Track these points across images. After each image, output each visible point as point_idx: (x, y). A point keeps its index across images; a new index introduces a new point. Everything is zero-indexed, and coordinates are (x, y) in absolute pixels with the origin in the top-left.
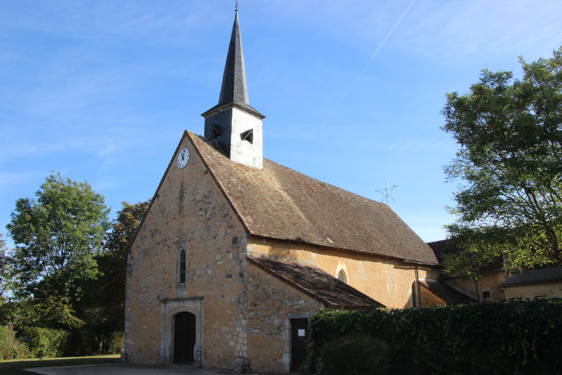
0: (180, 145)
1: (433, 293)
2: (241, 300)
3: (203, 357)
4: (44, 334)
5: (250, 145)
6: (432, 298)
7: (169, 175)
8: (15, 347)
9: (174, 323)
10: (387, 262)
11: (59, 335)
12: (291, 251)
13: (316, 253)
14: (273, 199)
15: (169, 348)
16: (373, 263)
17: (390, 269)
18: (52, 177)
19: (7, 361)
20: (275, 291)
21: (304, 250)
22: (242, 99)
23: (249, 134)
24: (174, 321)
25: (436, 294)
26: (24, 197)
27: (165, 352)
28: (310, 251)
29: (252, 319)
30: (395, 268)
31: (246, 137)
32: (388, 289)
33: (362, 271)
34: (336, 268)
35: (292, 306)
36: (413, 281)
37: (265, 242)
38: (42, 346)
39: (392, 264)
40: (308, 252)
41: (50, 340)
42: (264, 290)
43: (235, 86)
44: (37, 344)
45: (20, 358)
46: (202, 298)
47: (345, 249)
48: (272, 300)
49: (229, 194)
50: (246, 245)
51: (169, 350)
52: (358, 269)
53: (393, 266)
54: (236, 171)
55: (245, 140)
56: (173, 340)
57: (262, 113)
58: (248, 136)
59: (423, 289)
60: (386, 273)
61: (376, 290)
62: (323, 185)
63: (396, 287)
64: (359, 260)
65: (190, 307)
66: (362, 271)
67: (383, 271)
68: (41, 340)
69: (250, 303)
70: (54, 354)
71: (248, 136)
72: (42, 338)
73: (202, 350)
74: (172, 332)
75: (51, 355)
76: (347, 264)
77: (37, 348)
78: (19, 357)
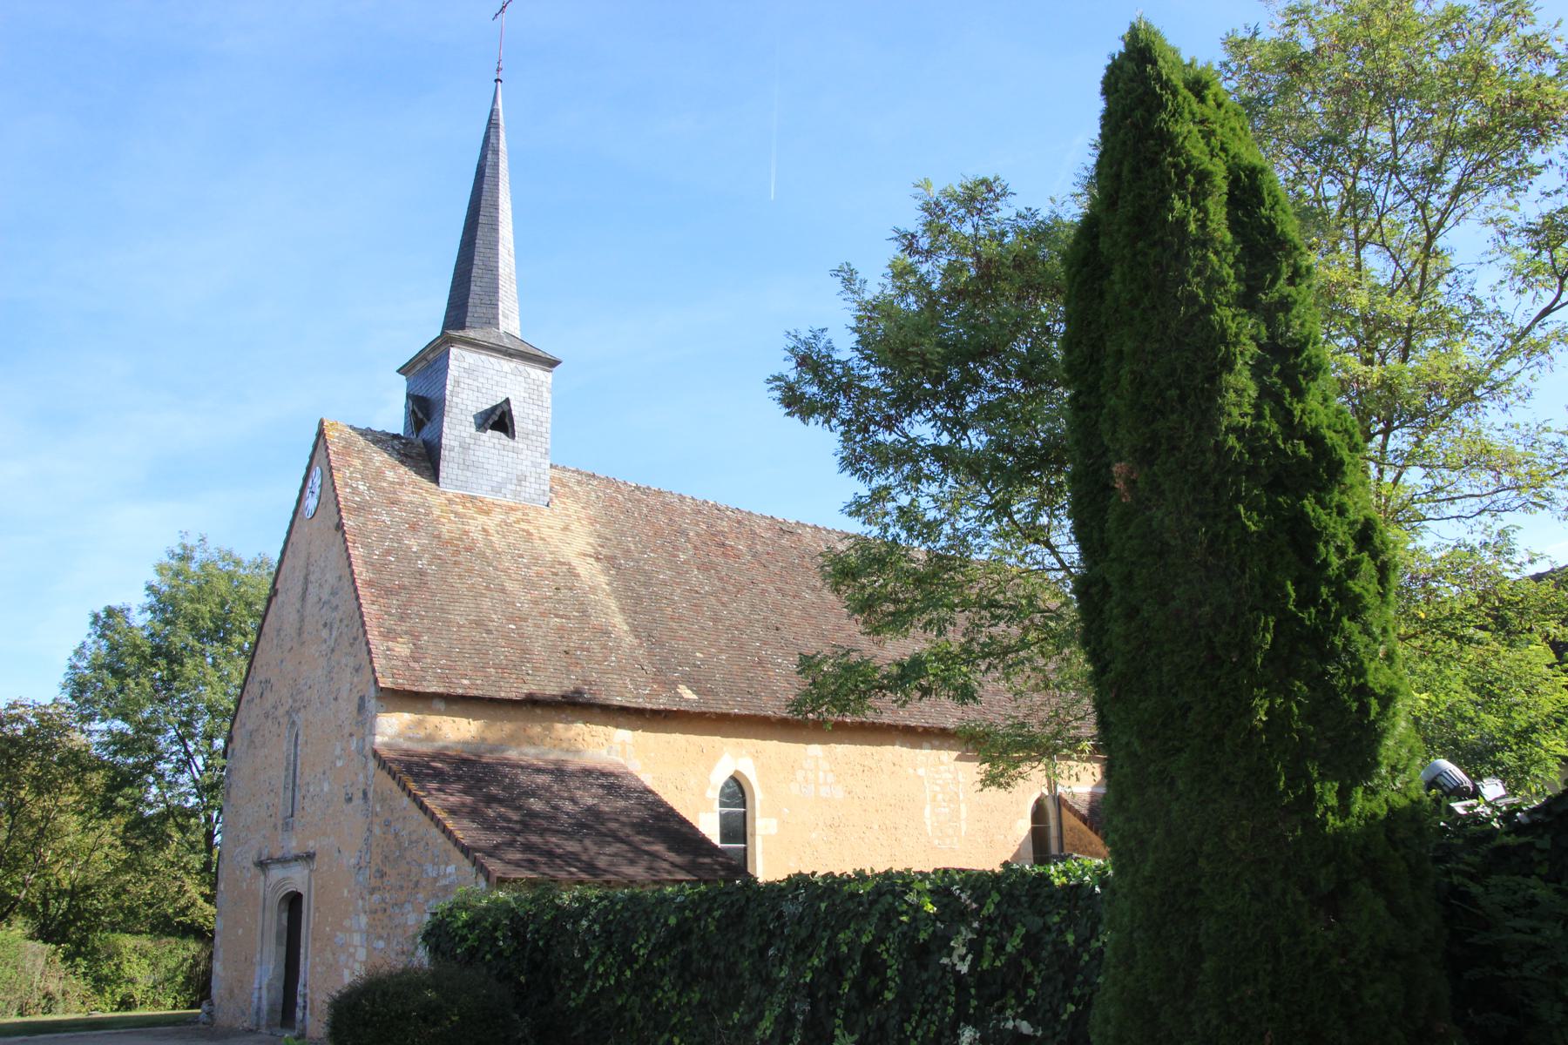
0: (312, 458)
1: (1091, 828)
2: (363, 864)
3: (308, 1012)
4: (135, 950)
5: (506, 442)
6: (1091, 844)
7: (293, 538)
8: (54, 986)
9: (285, 922)
10: (925, 744)
11: (182, 953)
12: (559, 726)
13: (634, 729)
14: (529, 585)
15: (269, 987)
16: (867, 749)
17: (942, 763)
18: (185, 547)
19: (177, 1011)
20: (414, 837)
21: (585, 722)
22: (493, 321)
23: (498, 412)
24: (285, 916)
25: (1096, 833)
26: (116, 603)
27: (260, 998)
28: (606, 725)
29: (376, 912)
30: (959, 759)
31: (491, 422)
32: (928, 822)
33: (821, 774)
34: (710, 769)
35: (436, 880)
36: (1036, 795)
37: (441, 706)
38: (132, 981)
39: (950, 748)
40: (601, 728)
41: (154, 965)
42: (396, 835)
43: (472, 288)
44: (115, 979)
45: (66, 1011)
46: (309, 857)
47: (736, 715)
48: (408, 863)
49: (370, 584)
50: (375, 717)
51: (269, 991)
52: (802, 768)
53: (955, 754)
54: (439, 517)
55: (489, 431)
56: (283, 967)
57: (551, 351)
58: (499, 420)
59: (1070, 820)
60: (919, 777)
61: (876, 827)
62: (784, 530)
63: (964, 815)
64: (809, 742)
65: (297, 878)
66: (821, 774)
67: (911, 771)
68: (126, 965)
69: (374, 870)
70: (170, 1002)
71: (499, 420)
72: (129, 961)
73: (308, 991)
74: (279, 943)
75: (156, 1003)
76: (756, 756)
77: (119, 986)
78: (60, 1010)
